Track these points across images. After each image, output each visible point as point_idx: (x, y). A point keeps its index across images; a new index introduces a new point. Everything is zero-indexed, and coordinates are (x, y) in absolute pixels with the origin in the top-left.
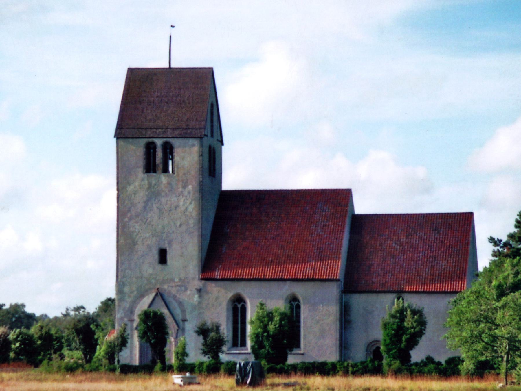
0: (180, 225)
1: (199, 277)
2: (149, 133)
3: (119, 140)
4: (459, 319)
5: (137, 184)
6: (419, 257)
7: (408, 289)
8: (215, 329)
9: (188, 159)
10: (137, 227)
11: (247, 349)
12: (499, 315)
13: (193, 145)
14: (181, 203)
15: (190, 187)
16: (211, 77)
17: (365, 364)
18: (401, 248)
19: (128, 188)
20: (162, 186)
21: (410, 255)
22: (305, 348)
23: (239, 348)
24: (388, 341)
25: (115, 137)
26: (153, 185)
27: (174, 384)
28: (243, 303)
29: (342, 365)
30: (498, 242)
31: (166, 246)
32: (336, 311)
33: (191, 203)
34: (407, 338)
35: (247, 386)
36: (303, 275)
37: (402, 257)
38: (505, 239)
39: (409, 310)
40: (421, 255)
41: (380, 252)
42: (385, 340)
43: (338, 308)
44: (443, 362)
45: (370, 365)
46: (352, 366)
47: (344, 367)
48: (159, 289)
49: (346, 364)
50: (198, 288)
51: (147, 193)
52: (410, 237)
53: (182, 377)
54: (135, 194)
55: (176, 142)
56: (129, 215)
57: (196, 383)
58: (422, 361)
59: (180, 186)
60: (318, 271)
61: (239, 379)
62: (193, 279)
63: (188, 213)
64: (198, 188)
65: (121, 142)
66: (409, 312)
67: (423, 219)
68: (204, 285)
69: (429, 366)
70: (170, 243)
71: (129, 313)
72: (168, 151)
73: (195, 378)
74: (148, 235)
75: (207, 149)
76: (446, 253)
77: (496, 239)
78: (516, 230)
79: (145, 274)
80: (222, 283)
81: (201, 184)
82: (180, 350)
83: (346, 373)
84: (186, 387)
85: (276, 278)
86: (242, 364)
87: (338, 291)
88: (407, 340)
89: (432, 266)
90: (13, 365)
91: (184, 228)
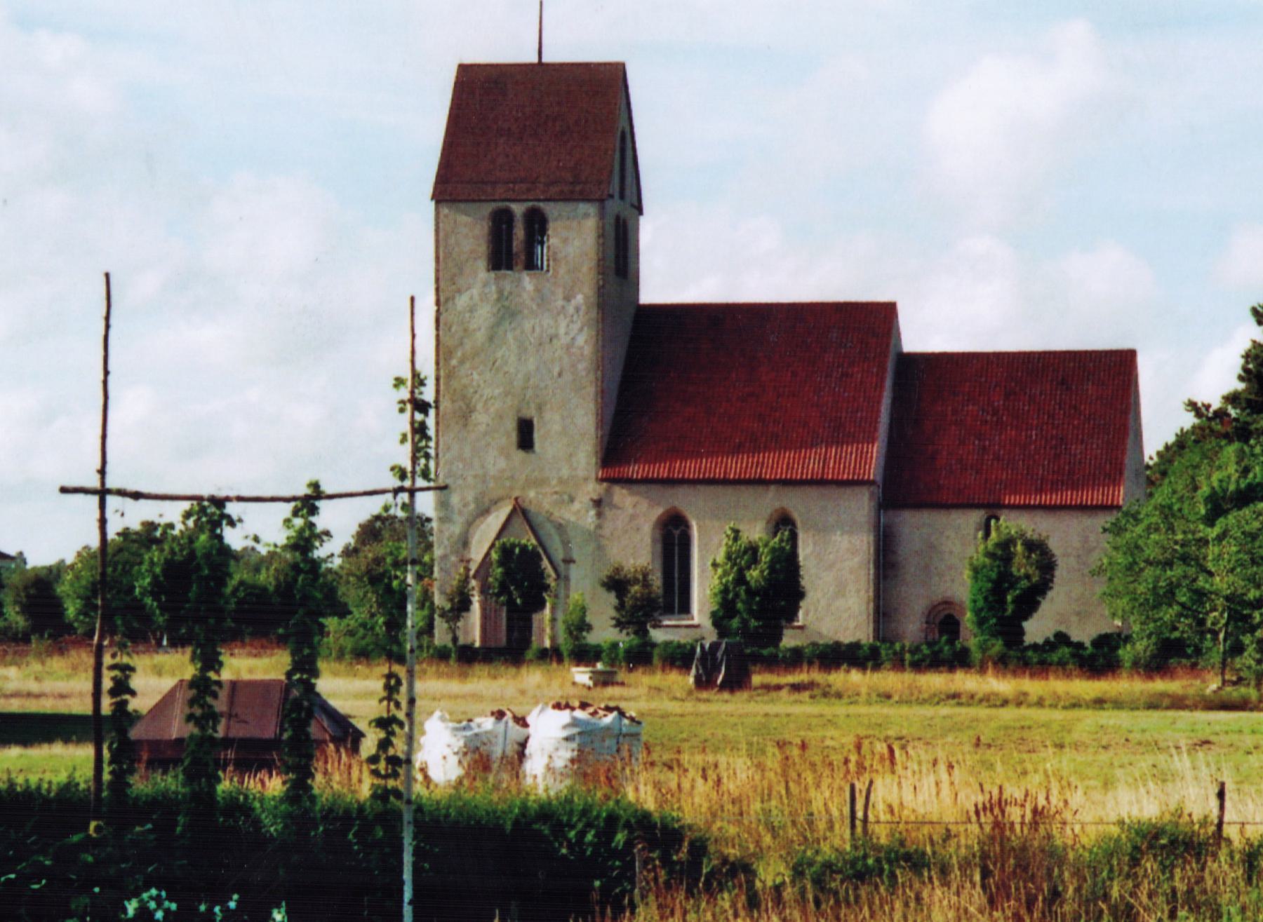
0: (560, 375)
1: (597, 474)
2: (500, 190)
3: (440, 205)
4: (1131, 560)
5: (475, 292)
6: (1031, 436)
7: (1010, 500)
8: (641, 577)
9: (577, 243)
10: (476, 376)
11: (693, 619)
12: (1212, 551)
13: (586, 215)
14: (562, 331)
15: (580, 298)
16: (621, 83)
17: (936, 648)
18: (995, 419)
19: (457, 300)
20: (525, 296)
21: (1013, 433)
22: (805, 619)
23: (676, 616)
24: (980, 603)
25: (432, 199)
26: (506, 293)
27: (574, 684)
28: (683, 528)
29: (890, 648)
30: (1203, 410)
31: (530, 412)
32: (869, 543)
33: (581, 330)
34: (1017, 597)
35: (716, 689)
36: (802, 473)
37: (997, 438)
38: (1216, 404)
39: (1019, 543)
40: (1034, 432)
41: (953, 427)
42: (975, 601)
43: (872, 538)
44: (1088, 644)
45: (946, 648)
46: (910, 651)
47: (895, 653)
48: (519, 500)
49: (897, 646)
50: (595, 497)
51: (495, 310)
52: (1012, 397)
53: (592, 672)
54: (471, 311)
55: (550, 209)
56: (459, 354)
57: (617, 684)
58: (1047, 642)
59: (560, 296)
60: (831, 465)
61: (701, 675)
62: (586, 479)
63: (574, 350)
64: (593, 300)
65: (445, 210)
66: (1019, 548)
67: (1038, 362)
68: (608, 491)
69: (1061, 651)
70: (540, 408)
71: (460, 545)
72: (537, 226)
73: (615, 673)
74: (497, 392)
75: (612, 221)
76: (1084, 429)
77: (1200, 405)
78: (1241, 386)
79: (492, 471)
80: (643, 488)
81: (601, 291)
82: (575, 617)
83: (899, 664)
84: (598, 689)
85: (796, 479)
86: (707, 646)
87: (872, 504)
88: (1017, 600)
89: (1055, 454)
90: (251, 645)
91: (568, 377)
